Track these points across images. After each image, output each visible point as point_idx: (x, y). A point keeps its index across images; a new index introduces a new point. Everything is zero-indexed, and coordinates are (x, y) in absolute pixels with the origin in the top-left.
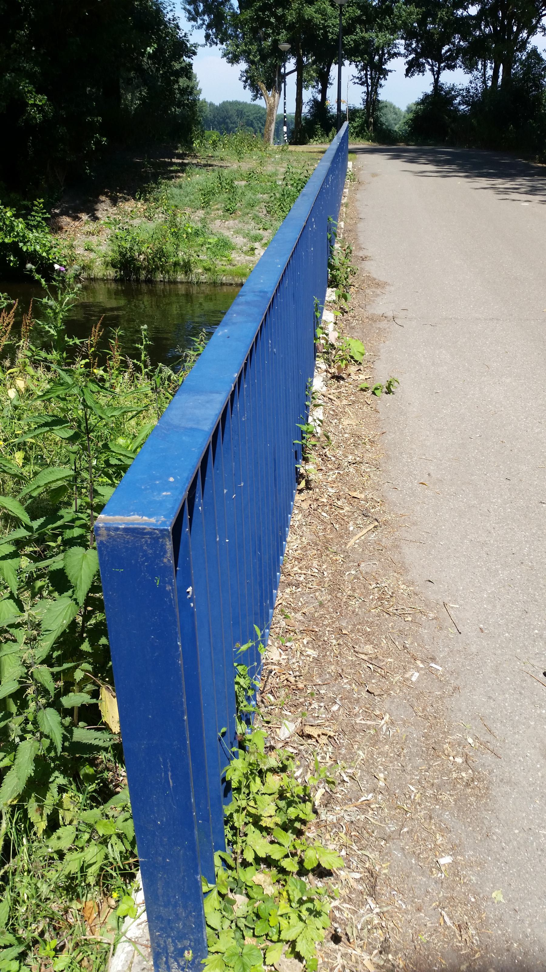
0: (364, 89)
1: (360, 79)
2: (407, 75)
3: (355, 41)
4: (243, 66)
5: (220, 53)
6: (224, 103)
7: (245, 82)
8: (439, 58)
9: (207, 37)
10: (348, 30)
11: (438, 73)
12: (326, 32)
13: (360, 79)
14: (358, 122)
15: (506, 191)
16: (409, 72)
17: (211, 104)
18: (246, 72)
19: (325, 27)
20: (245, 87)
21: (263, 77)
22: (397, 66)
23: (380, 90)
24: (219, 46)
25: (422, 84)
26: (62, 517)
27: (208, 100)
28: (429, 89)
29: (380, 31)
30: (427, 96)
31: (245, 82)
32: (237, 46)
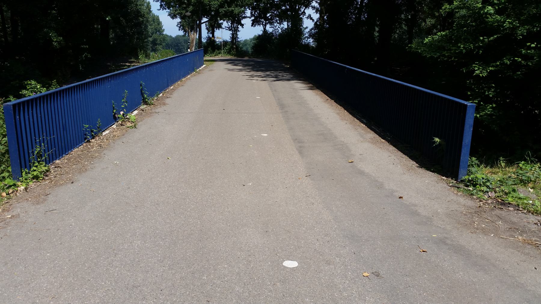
0: (231, 32)
1: (229, 28)
2: (252, 26)
3: (225, 11)
4: (178, 20)
5: (167, 14)
6: (177, 36)
7: (180, 27)
8: (266, 19)
9: (161, 6)
10: (221, 6)
11: (265, 26)
12: (210, 7)
13: (229, 28)
14: (228, 47)
15: (252, 76)
16: (253, 25)
17: (171, 37)
18: (180, 22)
19: (209, 5)
20: (179, 30)
21: (190, 24)
22: (247, 22)
23: (238, 33)
24: (167, 10)
25: (258, 30)
26: (24, 96)
27: (169, 34)
28: (261, 33)
29: (236, 7)
30: (259, 36)
31: (180, 27)
32: (176, 11)
